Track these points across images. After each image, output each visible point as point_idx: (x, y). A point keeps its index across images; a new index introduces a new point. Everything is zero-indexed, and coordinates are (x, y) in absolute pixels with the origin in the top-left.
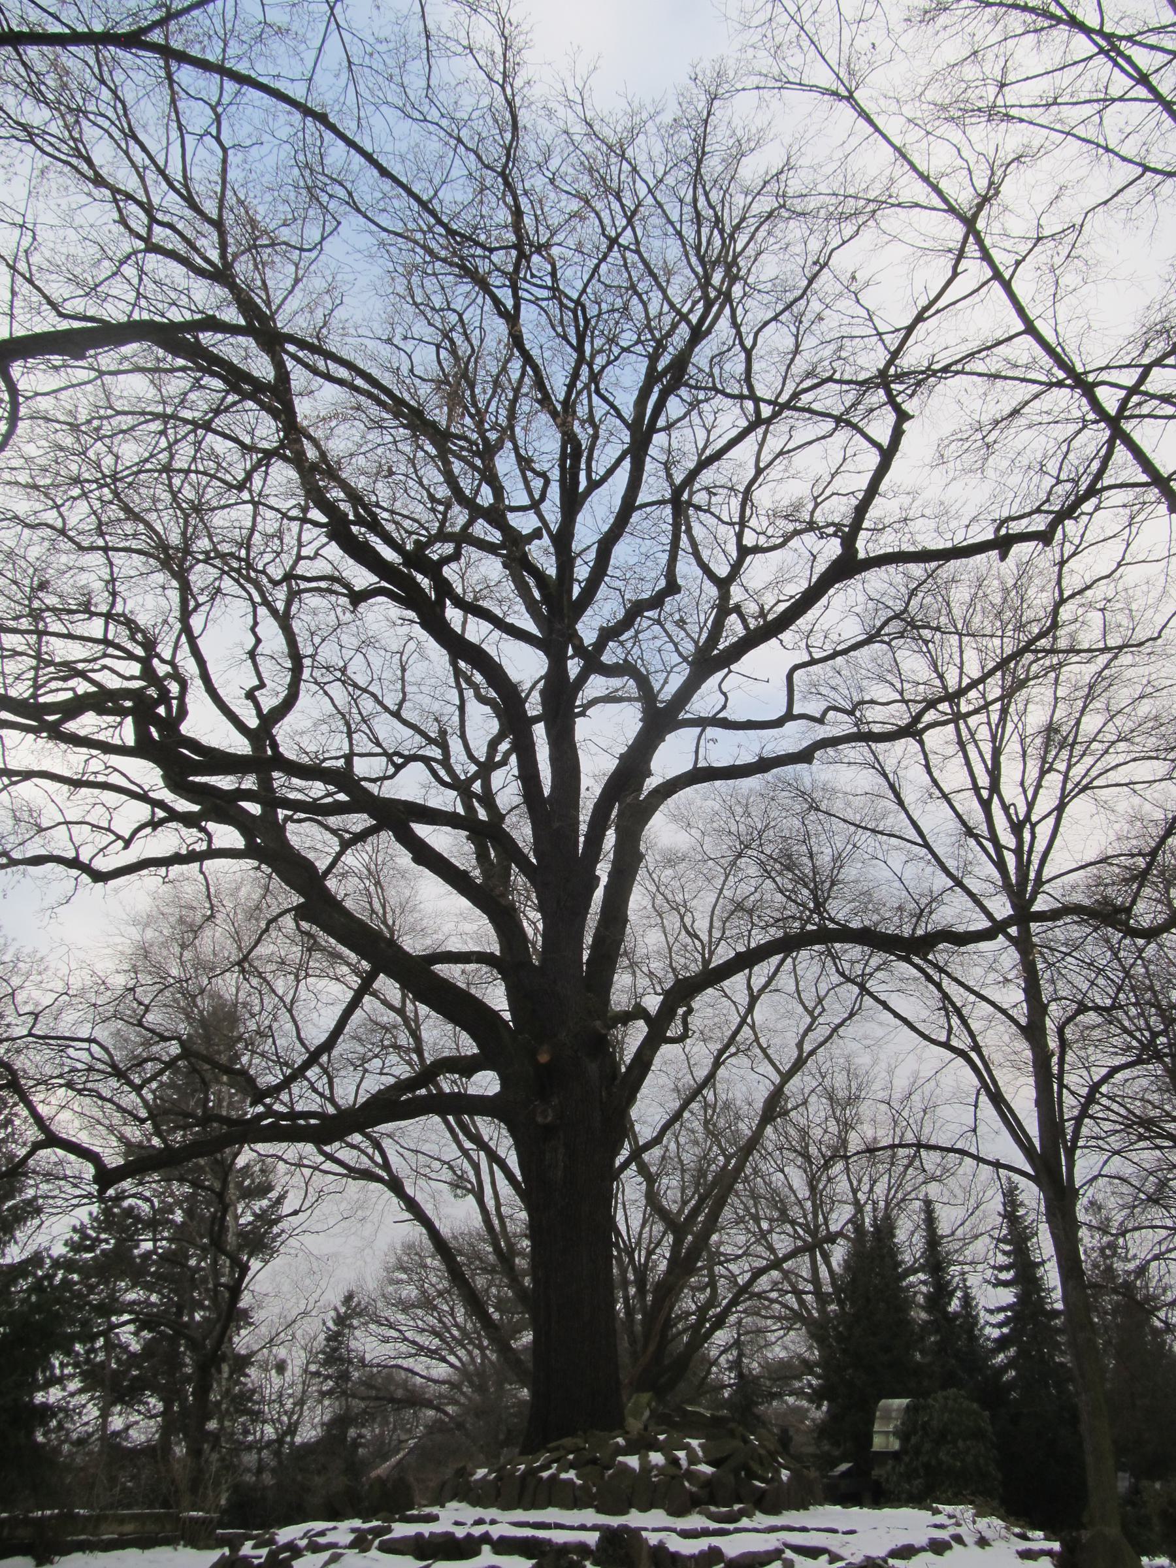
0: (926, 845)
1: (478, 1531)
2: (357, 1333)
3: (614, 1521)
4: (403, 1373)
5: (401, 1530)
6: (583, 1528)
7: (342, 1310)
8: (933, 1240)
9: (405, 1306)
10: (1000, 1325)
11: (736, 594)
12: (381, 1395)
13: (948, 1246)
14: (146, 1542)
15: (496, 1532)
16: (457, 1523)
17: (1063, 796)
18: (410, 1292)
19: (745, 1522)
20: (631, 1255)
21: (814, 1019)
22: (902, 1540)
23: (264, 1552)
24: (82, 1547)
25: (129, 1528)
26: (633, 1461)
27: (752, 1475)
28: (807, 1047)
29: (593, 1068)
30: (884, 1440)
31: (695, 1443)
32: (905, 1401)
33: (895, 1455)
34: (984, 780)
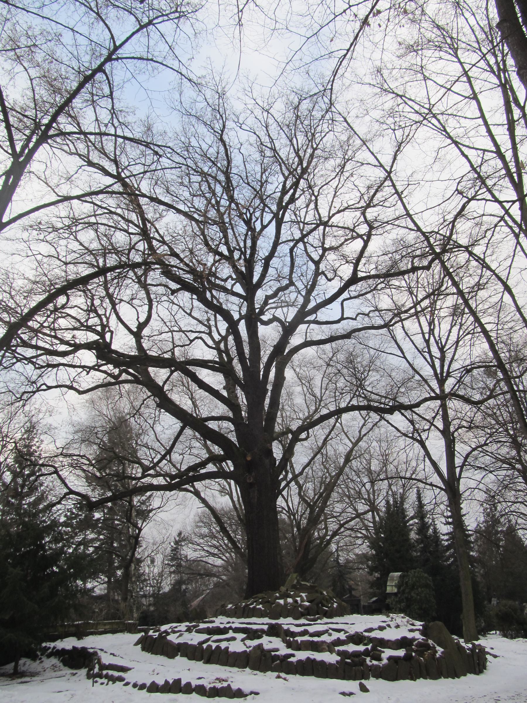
0: (405, 357)
1: (228, 626)
2: (184, 548)
3: (274, 622)
4: (204, 563)
5: (202, 626)
6: (263, 624)
7: (177, 539)
8: (421, 505)
9: (202, 536)
10: (447, 540)
11: (322, 267)
12: (194, 572)
13: (428, 508)
14: (114, 632)
15: (234, 626)
16: (221, 623)
17: (458, 338)
18: (205, 531)
19: (319, 621)
20: (294, 516)
21: (366, 421)
22: (369, 626)
23: (157, 634)
24: (92, 633)
25: (107, 627)
26: (282, 602)
27: (323, 605)
28: (363, 433)
29: (267, 461)
30: (391, 588)
31: (303, 595)
32: (399, 573)
33: (395, 594)
34: (426, 329)
